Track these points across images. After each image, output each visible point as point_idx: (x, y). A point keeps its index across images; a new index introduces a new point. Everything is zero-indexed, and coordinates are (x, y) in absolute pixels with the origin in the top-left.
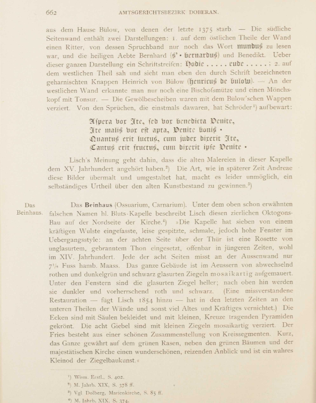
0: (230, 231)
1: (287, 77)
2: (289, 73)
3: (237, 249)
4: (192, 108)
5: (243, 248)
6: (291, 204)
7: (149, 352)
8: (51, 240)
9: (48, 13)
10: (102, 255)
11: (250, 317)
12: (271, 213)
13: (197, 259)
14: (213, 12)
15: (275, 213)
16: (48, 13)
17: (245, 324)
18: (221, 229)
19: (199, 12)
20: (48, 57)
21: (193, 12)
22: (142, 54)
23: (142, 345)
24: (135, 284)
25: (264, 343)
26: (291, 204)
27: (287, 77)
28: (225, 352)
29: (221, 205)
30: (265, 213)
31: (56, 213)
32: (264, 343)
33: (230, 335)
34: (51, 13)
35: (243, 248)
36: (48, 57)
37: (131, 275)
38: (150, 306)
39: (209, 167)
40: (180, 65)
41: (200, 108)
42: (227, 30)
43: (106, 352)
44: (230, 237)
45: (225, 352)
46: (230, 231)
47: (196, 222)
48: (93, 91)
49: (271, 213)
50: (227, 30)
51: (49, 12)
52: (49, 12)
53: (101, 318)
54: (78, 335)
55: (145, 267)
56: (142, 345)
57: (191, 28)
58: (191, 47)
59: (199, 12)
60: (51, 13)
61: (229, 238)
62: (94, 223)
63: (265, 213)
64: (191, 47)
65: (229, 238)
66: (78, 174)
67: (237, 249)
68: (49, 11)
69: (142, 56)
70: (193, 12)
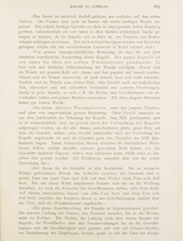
6: (159, 17)
9: (155, 7)
12: (59, 194)
14: (105, 7)
16: (155, 7)
19: (97, 6)
21: (94, 7)
26: (159, 17)
28: (25, 22)
29: (147, 17)
30: (113, 113)
31: (147, 21)
34: (157, 7)
45: (25, 22)
47: (93, 208)
49: (59, 194)
53: (67, 27)
59: (97, 6)
60: (157, 7)
61: (88, 26)
63: (113, 113)
65: (88, 26)
68: (156, 6)
70: (94, 7)
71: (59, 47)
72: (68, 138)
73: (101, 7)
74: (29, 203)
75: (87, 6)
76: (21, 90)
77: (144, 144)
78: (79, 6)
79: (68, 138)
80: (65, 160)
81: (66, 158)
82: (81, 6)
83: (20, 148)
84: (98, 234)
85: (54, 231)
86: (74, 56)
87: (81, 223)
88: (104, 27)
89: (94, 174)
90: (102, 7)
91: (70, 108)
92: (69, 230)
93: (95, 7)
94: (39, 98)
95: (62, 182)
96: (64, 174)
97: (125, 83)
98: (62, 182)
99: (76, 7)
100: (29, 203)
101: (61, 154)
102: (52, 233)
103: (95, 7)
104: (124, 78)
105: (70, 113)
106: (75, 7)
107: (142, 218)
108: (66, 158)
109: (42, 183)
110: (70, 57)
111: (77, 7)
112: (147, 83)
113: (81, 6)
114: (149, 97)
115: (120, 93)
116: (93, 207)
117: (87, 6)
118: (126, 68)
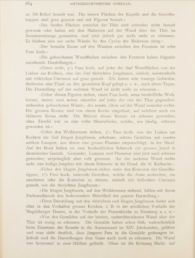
0: (33, 238)
3: (167, 58)
4: (168, 122)
5: (141, 42)
7: (107, 47)
10: (151, 227)
11: (152, 228)
17: (53, 222)
18: (108, 67)
25: (160, 111)
32: (160, 111)
33: (56, 111)
35: (141, 42)
38: (60, 135)
39: (139, 120)
40: (174, 116)
41: (170, 191)
42: (32, 196)
44: (172, 231)
46: (33, 238)
48: (99, 90)
50: (32, 196)
55: (119, 37)
57: (77, 227)
58: (122, 239)
62: (142, 212)
64: (122, 239)
65: (122, 243)
67: (167, 58)
70: (116, 4)
72: (116, 228)
76: (28, 113)
77: (33, 106)
78: (105, 58)
79: (116, 228)
80: (70, 13)
81: (106, 180)
83: (28, 100)
85: (137, 44)
86: (174, 220)
87: (39, 158)
91: (72, 57)
92: (65, 167)
95: (99, 46)
96: (156, 159)
98: (99, 46)
100: (112, 25)
101: (100, 21)
102: (135, 47)
103: (117, 4)
104: (84, 20)
105: (113, 36)
107: (70, 47)
108: (106, 180)
109: (87, 20)
110: (72, 196)
117: (153, 14)
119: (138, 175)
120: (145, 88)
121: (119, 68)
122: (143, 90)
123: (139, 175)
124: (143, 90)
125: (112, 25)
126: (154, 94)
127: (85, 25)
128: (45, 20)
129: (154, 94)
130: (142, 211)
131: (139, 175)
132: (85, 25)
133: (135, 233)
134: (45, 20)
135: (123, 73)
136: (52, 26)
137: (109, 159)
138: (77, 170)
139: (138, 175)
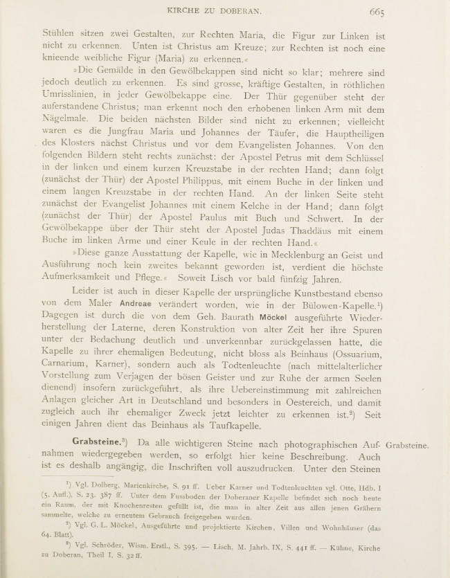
1: (379, 92)
2: (382, 86)
8: (235, 390)
10: (80, 104)
13: (351, 113)
14: (253, 11)
15: (305, 445)
20: (45, 131)
22: (294, 455)
23: (219, 86)
24: (372, 343)
27: (379, 92)
28: (101, 58)
36: (45, 131)
37: (352, 294)
43: (118, 316)
51: (374, 12)
52: (374, 12)
54: (241, 342)
56: (219, 86)
60: (377, 13)
62: (45, 119)
66: (207, 188)
68: (375, 10)
69: (294, 458)
71: (309, 158)
73: (242, 11)
74: (114, 216)
75: (208, 11)
82: (194, 10)
84: (205, 528)
88: (145, 293)
89: (199, 414)
90: (245, 11)
93: (229, 11)
94: (346, 86)
97: (210, 109)
99: (181, 11)
100: (114, 216)
106: (179, 10)
111: (185, 10)
112: (263, 109)
113: (194, 10)
114: (71, 92)
115: (148, 96)
116: (207, 250)
117: (208, 11)
118: (47, 155)
119: (125, 242)
120: (179, 105)
121: (67, 303)
122: (174, 108)
123: (128, 241)
124: (174, 108)
125: (108, 179)
126: (229, 424)
127: (186, 35)
128: (202, 84)
129: (229, 424)
130: (47, 116)
131: (128, 241)
132: (186, 35)
133: (135, 353)
134: (202, 84)
135: (130, 129)
136: (230, 403)
137: (337, 280)
138: (260, 230)
139: (125, 242)
